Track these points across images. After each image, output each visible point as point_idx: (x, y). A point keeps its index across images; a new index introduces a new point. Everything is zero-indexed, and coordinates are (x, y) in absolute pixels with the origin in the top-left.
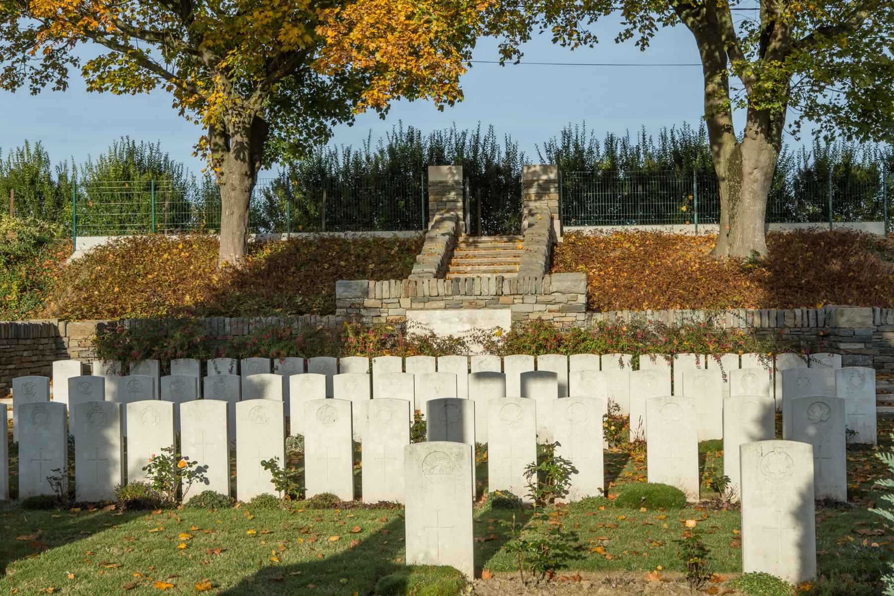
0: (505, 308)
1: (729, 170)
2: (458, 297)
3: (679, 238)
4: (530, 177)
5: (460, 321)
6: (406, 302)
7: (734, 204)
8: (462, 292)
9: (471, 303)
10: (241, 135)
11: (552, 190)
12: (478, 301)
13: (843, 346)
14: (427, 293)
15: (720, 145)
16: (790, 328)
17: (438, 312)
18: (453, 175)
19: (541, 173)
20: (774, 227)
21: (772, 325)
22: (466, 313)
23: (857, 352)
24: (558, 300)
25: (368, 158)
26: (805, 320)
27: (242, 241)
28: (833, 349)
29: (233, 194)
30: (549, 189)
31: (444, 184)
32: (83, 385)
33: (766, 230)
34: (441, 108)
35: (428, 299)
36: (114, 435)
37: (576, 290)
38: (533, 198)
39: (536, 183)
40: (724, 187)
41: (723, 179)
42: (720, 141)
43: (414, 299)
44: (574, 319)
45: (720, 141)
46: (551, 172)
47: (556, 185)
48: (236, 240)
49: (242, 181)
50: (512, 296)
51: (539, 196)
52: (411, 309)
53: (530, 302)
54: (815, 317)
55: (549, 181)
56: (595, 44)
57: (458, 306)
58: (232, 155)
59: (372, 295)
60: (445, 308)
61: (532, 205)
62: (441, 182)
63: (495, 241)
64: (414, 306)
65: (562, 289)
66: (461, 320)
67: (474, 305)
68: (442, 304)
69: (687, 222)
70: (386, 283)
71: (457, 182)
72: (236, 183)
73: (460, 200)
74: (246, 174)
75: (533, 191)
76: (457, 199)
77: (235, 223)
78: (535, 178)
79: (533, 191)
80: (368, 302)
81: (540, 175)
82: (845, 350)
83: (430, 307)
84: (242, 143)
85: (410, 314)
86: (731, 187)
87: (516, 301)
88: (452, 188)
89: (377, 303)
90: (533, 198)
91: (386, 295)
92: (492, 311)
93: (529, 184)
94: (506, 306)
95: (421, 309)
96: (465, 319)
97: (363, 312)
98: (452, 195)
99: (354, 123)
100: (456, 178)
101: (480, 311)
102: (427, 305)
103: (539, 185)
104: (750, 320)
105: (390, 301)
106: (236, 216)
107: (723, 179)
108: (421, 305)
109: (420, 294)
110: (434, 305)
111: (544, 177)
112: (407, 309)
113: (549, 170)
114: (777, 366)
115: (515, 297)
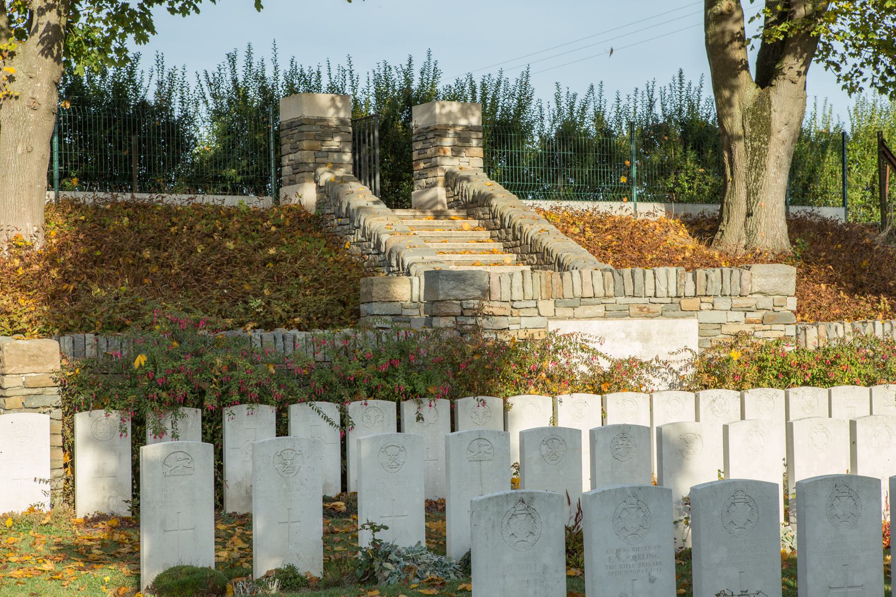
0: (688, 316)
2: (621, 300)
5: (626, 337)
6: (547, 307)
7: (759, 174)
8: (629, 291)
9: (641, 309)
10: (59, 14)
11: (474, 142)
12: (651, 306)
18: (338, 109)
19: (459, 115)
20: (793, 209)
22: (636, 325)
29: (32, 115)
31: (325, 123)
32: (389, 450)
33: (787, 213)
37: (784, 290)
40: (739, 148)
41: (739, 138)
42: (734, 82)
43: (559, 300)
44: (782, 334)
45: (734, 82)
46: (473, 115)
47: (480, 135)
50: (698, 299)
51: (457, 151)
53: (723, 307)
55: (469, 129)
57: (623, 314)
59: (496, 295)
60: (605, 317)
63: (414, 217)
64: (559, 312)
65: (767, 288)
66: (628, 335)
67: (646, 313)
68: (600, 310)
69: (625, 199)
71: (342, 122)
73: (348, 149)
75: (448, 141)
76: (343, 148)
77: (35, 168)
78: (451, 123)
81: (457, 118)
83: (582, 315)
84: (57, 27)
86: (754, 150)
87: (704, 306)
88: (337, 131)
92: (671, 321)
95: (569, 318)
98: (335, 143)
99: (178, 16)
100: (342, 115)
101: (655, 321)
102: (579, 311)
103: (456, 133)
105: (523, 305)
107: (739, 138)
108: (569, 312)
110: (588, 311)
111: (463, 122)
112: (549, 318)
113: (469, 112)
115: (703, 299)
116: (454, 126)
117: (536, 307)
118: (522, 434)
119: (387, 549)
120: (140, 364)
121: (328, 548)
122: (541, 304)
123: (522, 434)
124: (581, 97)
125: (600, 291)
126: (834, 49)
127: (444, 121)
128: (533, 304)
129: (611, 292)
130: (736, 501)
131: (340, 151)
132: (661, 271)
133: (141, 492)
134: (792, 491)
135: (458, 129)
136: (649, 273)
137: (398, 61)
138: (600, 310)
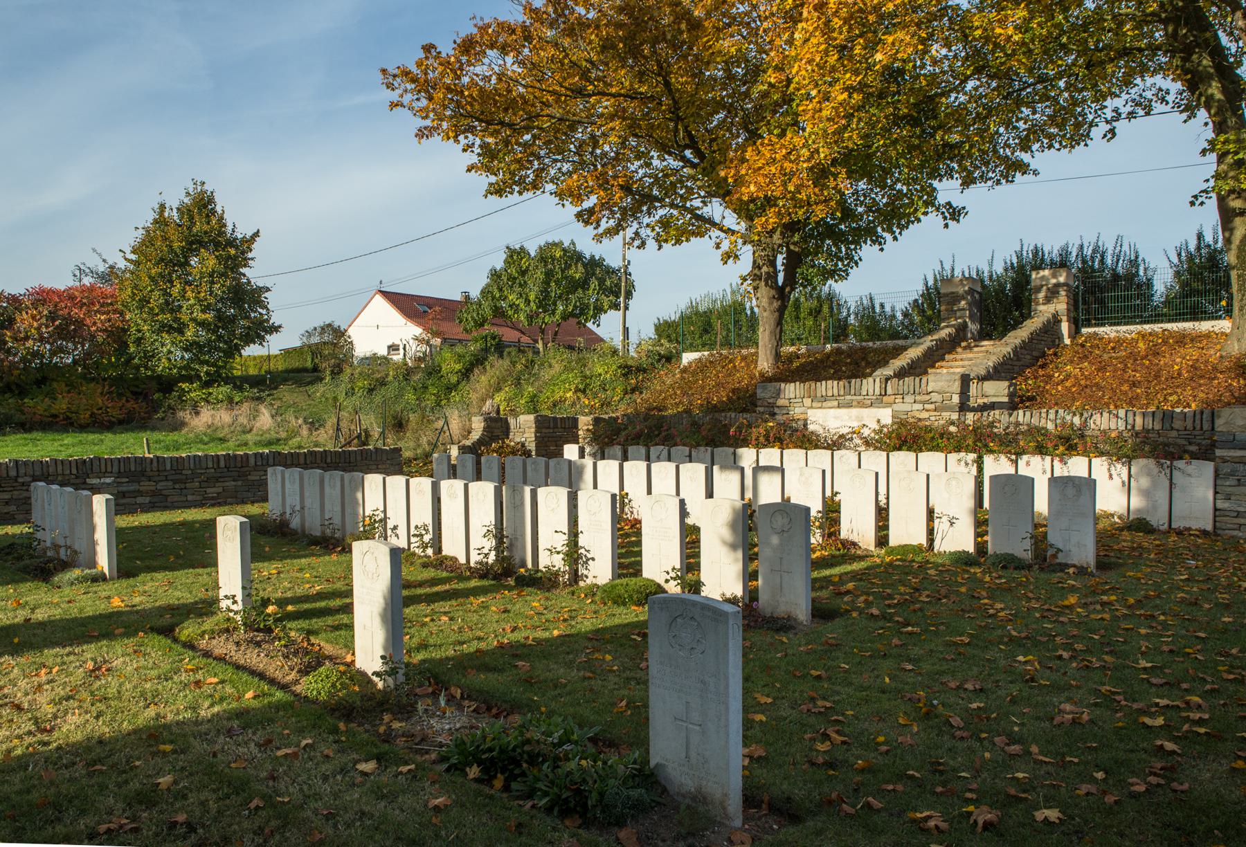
1: (1238, 257)
2: (848, 397)
3: (1208, 335)
4: (1038, 283)
6: (807, 402)
13: (1218, 452)
14: (824, 394)
15: (1232, 230)
16: (1178, 430)
17: (832, 410)
21: (1157, 427)
22: (854, 412)
23: (1237, 460)
24: (933, 400)
25: (991, 277)
26: (1198, 422)
27: (774, 352)
28: (1205, 454)
30: (1058, 293)
34: (946, 226)
35: (825, 399)
36: (359, 495)
37: (950, 390)
38: (1041, 300)
39: (1045, 288)
42: (1230, 226)
48: (768, 352)
49: (771, 303)
51: (1048, 300)
52: (812, 407)
54: (1210, 419)
56: (1089, 142)
57: (849, 405)
58: (763, 283)
59: (782, 396)
61: (1041, 308)
62: (953, 293)
64: (814, 404)
66: (850, 417)
67: (861, 405)
68: (836, 403)
70: (793, 384)
72: (766, 305)
74: (774, 297)
75: (1041, 295)
79: (1041, 295)
80: (781, 402)
82: (1222, 458)
85: (810, 412)
88: (963, 298)
89: (786, 402)
90: (1041, 300)
91: (792, 396)
93: (1039, 289)
94: (889, 405)
96: (854, 418)
97: (776, 410)
102: (824, 404)
103: (1048, 289)
104: (1130, 420)
106: (767, 332)
108: (820, 405)
109: (819, 395)
111: (1054, 281)
114: (1132, 473)
118: (991, 477)
123: (991, 477)
124: (1192, 247)
125: (836, 392)
126: (884, 246)
129: (842, 393)
132: (830, 382)
136: (917, 380)
137: (1089, 241)
138: (836, 403)
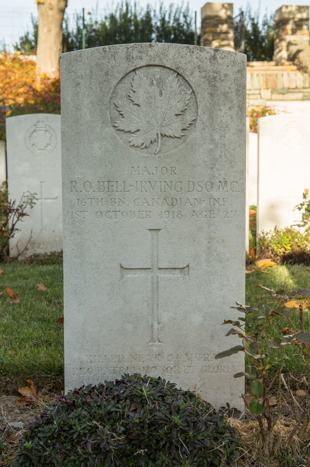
6: (266, 94)
19: (296, 12)
31: (218, 18)
51: (294, 32)
60: (303, 100)
75: (289, 27)
102: (286, 96)
108: (280, 97)
110: (292, 96)
116: (293, 18)
117: (260, 94)
119: (32, 93)
120: (146, 145)
121: (61, 283)
122: (263, 92)
127: (286, 16)
128: (258, 92)
130: (37, 129)
131: (227, 33)
133: (58, 57)
134: (92, 445)
135: (296, 20)
